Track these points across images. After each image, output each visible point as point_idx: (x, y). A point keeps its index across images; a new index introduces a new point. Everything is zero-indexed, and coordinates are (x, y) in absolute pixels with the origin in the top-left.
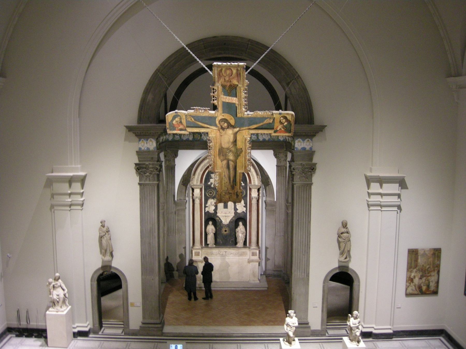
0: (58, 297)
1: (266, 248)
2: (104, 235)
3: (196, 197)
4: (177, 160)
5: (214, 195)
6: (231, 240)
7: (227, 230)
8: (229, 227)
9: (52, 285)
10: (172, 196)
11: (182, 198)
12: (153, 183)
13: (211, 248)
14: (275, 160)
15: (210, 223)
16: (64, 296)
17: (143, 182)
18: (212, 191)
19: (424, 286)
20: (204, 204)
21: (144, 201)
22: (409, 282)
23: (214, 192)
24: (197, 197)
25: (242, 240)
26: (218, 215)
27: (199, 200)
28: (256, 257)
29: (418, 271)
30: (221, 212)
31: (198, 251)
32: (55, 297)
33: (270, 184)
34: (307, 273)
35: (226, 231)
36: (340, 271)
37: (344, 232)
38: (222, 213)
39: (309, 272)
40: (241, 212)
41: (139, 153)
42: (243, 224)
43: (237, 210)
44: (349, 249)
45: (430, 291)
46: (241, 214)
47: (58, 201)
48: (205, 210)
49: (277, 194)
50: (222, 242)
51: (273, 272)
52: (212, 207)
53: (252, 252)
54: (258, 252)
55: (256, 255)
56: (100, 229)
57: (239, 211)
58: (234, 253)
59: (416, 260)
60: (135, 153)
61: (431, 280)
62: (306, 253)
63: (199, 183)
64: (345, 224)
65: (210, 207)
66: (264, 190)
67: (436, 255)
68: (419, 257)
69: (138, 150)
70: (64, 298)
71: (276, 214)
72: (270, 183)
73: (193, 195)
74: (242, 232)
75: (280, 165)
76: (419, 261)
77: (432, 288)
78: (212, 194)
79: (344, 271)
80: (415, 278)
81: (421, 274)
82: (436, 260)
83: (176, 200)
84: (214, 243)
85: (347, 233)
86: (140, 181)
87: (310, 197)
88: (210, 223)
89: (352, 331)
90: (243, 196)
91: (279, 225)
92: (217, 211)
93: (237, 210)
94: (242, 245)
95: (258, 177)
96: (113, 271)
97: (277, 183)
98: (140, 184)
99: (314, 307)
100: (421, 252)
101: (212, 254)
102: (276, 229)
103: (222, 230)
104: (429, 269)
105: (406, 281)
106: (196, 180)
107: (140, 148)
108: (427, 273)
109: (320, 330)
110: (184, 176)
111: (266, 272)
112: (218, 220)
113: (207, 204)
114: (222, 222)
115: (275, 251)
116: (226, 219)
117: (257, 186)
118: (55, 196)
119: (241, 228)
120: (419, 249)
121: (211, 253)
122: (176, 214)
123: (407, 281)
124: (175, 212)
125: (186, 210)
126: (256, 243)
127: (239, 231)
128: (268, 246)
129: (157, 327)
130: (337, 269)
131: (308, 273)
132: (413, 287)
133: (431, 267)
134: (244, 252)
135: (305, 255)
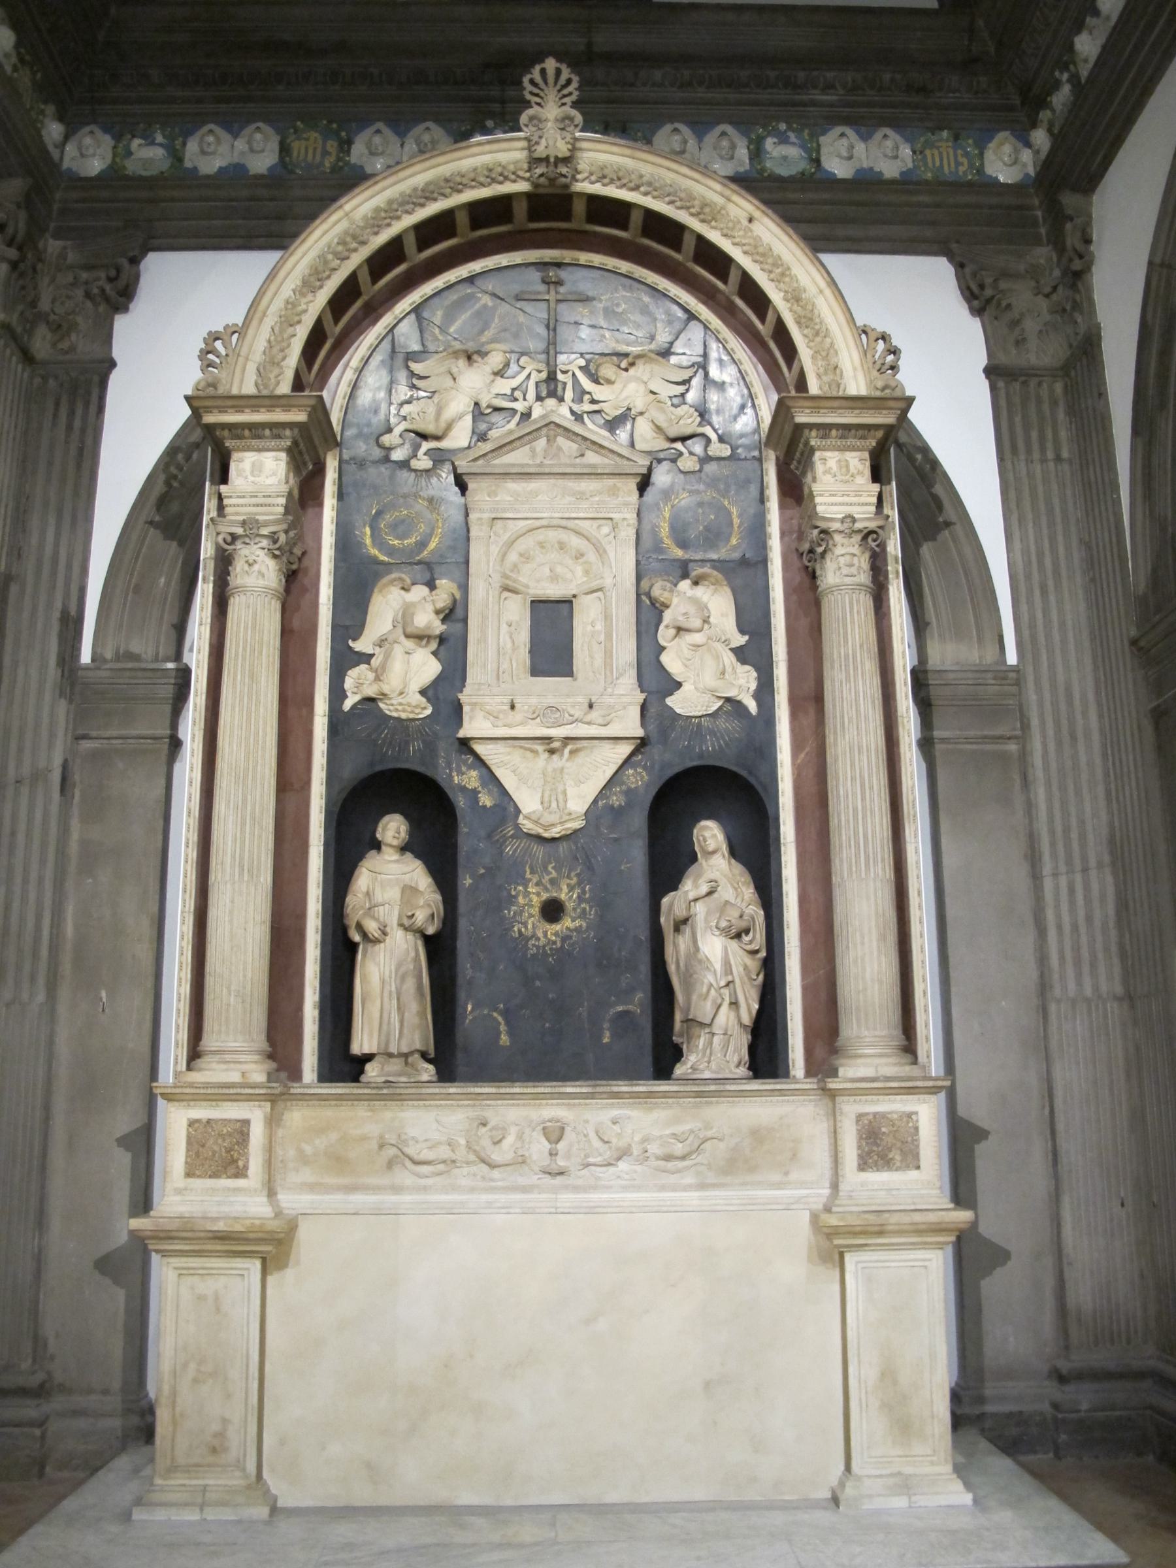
4: (121, 323)
7: (569, 905)
8: (590, 868)
13: (390, 1093)
14: (974, 328)
20: (335, 627)
25: (734, 1004)
28: (913, 1174)
30: (498, 702)
31: (232, 1112)
33: (948, 524)
38: (518, 716)
42: (734, 852)
46: (712, 733)
48: (337, 693)
49: (1024, 607)
50: (511, 1033)
51: (1053, 1391)
53: (860, 1117)
55: (912, 1159)
58: (645, 1140)
65: (387, 656)
72: (953, 517)
83: (86, 657)
91: (1072, 891)
97: (1012, 494)
101: (390, 1165)
110: (180, 457)
111: (981, 1400)
113: (357, 630)
114: (518, 811)
119: (710, 874)
124: (65, 766)
127: (700, 909)
134: (758, 1135)
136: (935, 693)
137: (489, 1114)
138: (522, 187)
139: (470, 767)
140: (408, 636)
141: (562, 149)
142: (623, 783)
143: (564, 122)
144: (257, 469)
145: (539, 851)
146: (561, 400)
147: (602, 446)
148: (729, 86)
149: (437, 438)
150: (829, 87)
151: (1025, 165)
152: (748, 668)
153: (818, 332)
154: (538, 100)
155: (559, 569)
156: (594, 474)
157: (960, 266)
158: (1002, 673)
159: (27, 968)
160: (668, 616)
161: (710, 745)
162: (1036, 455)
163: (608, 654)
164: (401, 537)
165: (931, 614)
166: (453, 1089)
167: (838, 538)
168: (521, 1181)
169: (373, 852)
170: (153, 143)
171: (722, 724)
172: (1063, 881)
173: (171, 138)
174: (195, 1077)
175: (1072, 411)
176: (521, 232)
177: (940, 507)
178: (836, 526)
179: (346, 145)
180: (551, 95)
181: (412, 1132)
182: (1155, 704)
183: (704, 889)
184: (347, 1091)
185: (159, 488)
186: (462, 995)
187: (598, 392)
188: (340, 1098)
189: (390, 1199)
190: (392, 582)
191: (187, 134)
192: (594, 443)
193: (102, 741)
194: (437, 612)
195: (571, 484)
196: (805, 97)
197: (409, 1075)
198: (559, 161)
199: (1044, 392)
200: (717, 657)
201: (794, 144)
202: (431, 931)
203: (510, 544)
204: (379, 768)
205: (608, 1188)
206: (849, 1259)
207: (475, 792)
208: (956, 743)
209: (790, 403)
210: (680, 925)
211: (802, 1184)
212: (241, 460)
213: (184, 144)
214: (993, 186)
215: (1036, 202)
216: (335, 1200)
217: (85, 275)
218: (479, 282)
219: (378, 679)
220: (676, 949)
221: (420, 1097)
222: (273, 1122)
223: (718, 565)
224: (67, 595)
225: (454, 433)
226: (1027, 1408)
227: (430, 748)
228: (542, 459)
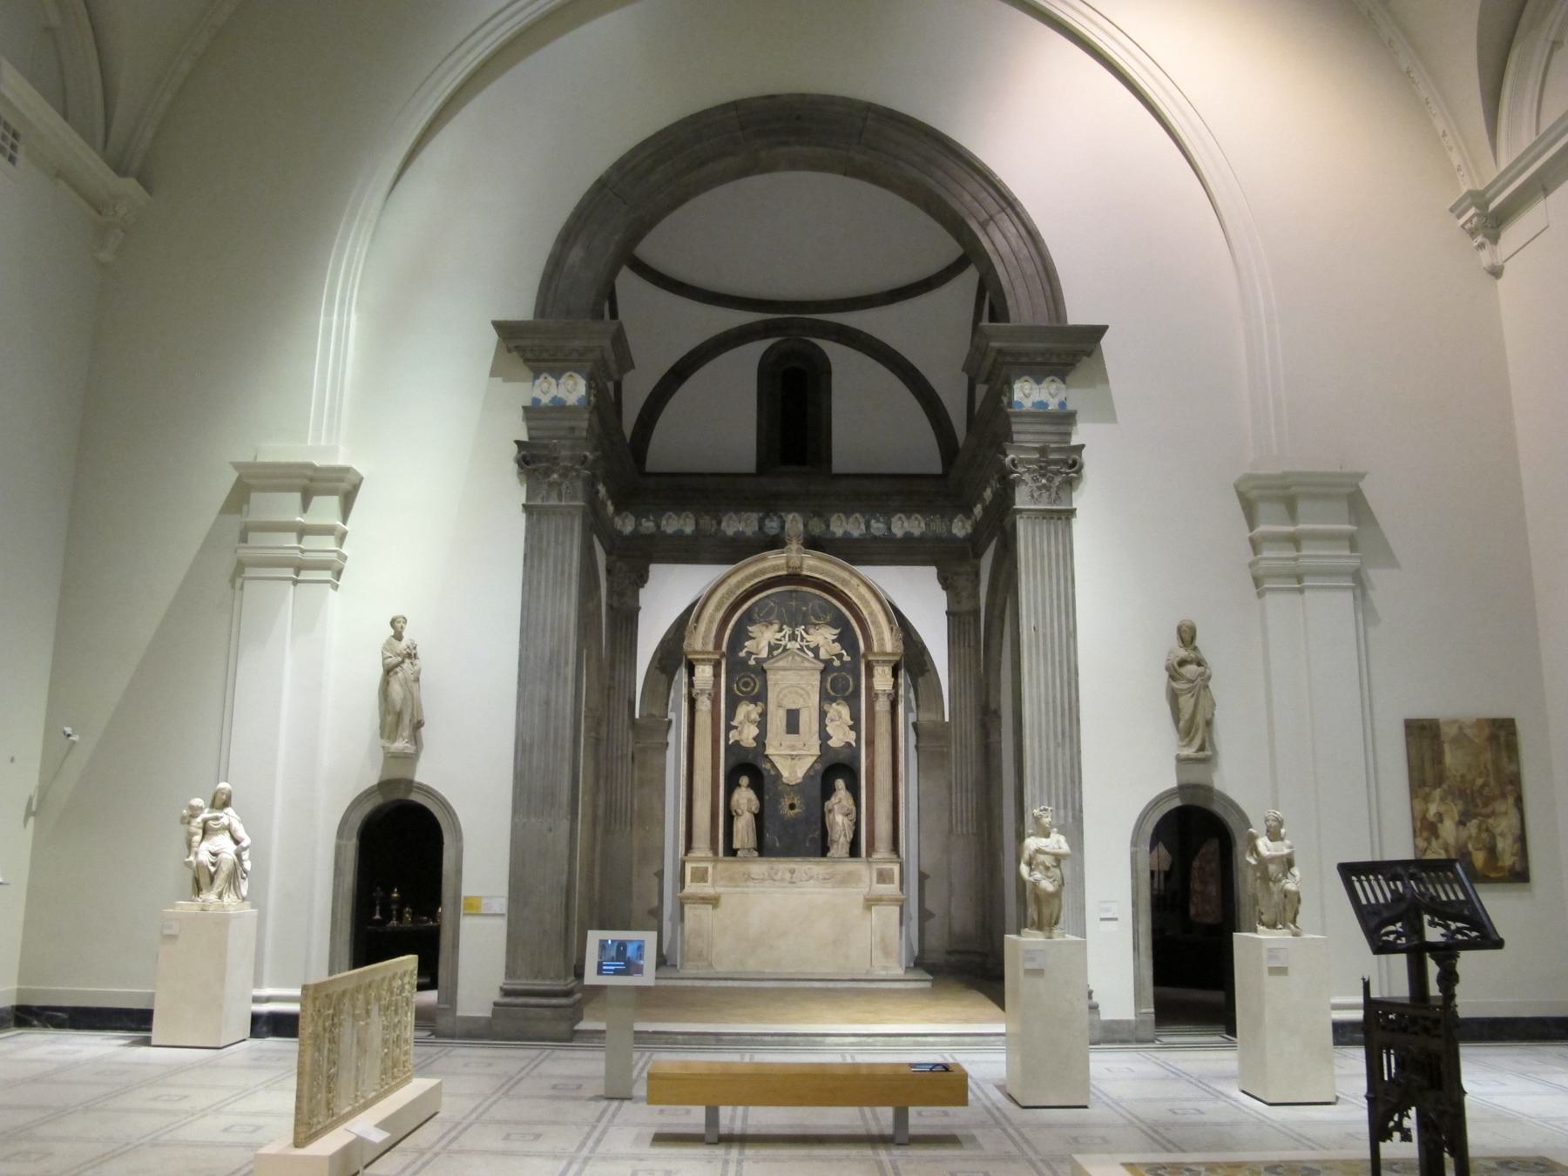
0: (213, 859)
1: (922, 877)
2: (398, 665)
3: (701, 690)
4: (642, 591)
5: (756, 690)
6: (811, 836)
7: (797, 805)
9: (199, 819)
10: (626, 703)
11: (655, 711)
12: (571, 506)
13: (746, 860)
14: (943, 596)
15: (744, 780)
16: (235, 857)
17: (538, 502)
18: (753, 680)
19: (1477, 849)
21: (536, 563)
22: (1425, 834)
24: (702, 691)
25: (845, 836)
26: (769, 751)
27: (709, 699)
28: (891, 886)
29: (1450, 798)
30: (776, 743)
31: (703, 865)
32: (205, 857)
33: (928, 670)
34: (1073, 809)
35: (792, 807)
36: (1185, 803)
37: (1189, 659)
38: (782, 748)
39: (1081, 806)
40: (843, 744)
41: (532, 412)
42: (848, 788)
43: (830, 737)
44: (1209, 716)
45: (1502, 868)
47: (261, 548)
48: (727, 739)
52: (749, 727)
53: (878, 869)
54: (896, 868)
55: (892, 881)
56: (387, 646)
57: (835, 742)
58: (818, 874)
59: (1438, 758)
60: (520, 413)
61: (1498, 830)
62: (1067, 740)
63: (710, 647)
64: (1187, 630)
66: (912, 690)
67: (1502, 740)
68: (1447, 747)
69: (528, 403)
70: (235, 864)
73: (691, 684)
76: (1449, 759)
77: (1508, 859)
79: (1199, 802)
80: (1441, 821)
81: (1460, 805)
82: (1505, 760)
83: (637, 716)
85: (1199, 664)
86: (528, 498)
87: (1068, 542)
88: (744, 780)
89: (1268, 885)
90: (847, 693)
93: (830, 737)
94: (844, 851)
95: (892, 629)
96: (416, 797)
98: (527, 508)
99: (1102, 919)
100: (1448, 732)
102: (951, 814)
104: (1486, 790)
105: (1415, 831)
107: (536, 401)
108: (1480, 805)
109: (1132, 1021)
114: (782, 776)
115: (951, 885)
116: (795, 765)
117: (889, 654)
118: (251, 535)
120: (1441, 721)
121: (744, 874)
122: (636, 761)
123: (1418, 833)
125: (668, 752)
126: (891, 842)
128: (927, 871)
129: (554, 1007)
130: (1175, 794)
131: (1077, 807)
132: (1439, 854)
133: (1492, 782)
134: (850, 874)
135: (1064, 746)
138: (784, 573)
141: (798, 563)
143: (798, 551)
145: (788, 789)
146: (796, 641)
148: (839, 578)
156: (806, 669)
157: (938, 569)
158: (944, 725)
159: (623, 819)
160: (829, 715)
161: (841, 757)
162: (962, 644)
163: (810, 728)
164: (746, 688)
165: (920, 703)
166: (764, 859)
167: (880, 696)
177: (926, 665)
179: (719, 523)
180: (794, 542)
183: (837, 801)
186: (765, 831)
189: (746, 890)
202: (756, 812)
203: (780, 692)
206: (873, 908)
207: (769, 770)
210: (830, 811)
211: (861, 888)
214: (954, 539)
219: (740, 734)
221: (755, 861)
222: (714, 868)
224: (630, 691)
225: (763, 652)
228: (794, 546)
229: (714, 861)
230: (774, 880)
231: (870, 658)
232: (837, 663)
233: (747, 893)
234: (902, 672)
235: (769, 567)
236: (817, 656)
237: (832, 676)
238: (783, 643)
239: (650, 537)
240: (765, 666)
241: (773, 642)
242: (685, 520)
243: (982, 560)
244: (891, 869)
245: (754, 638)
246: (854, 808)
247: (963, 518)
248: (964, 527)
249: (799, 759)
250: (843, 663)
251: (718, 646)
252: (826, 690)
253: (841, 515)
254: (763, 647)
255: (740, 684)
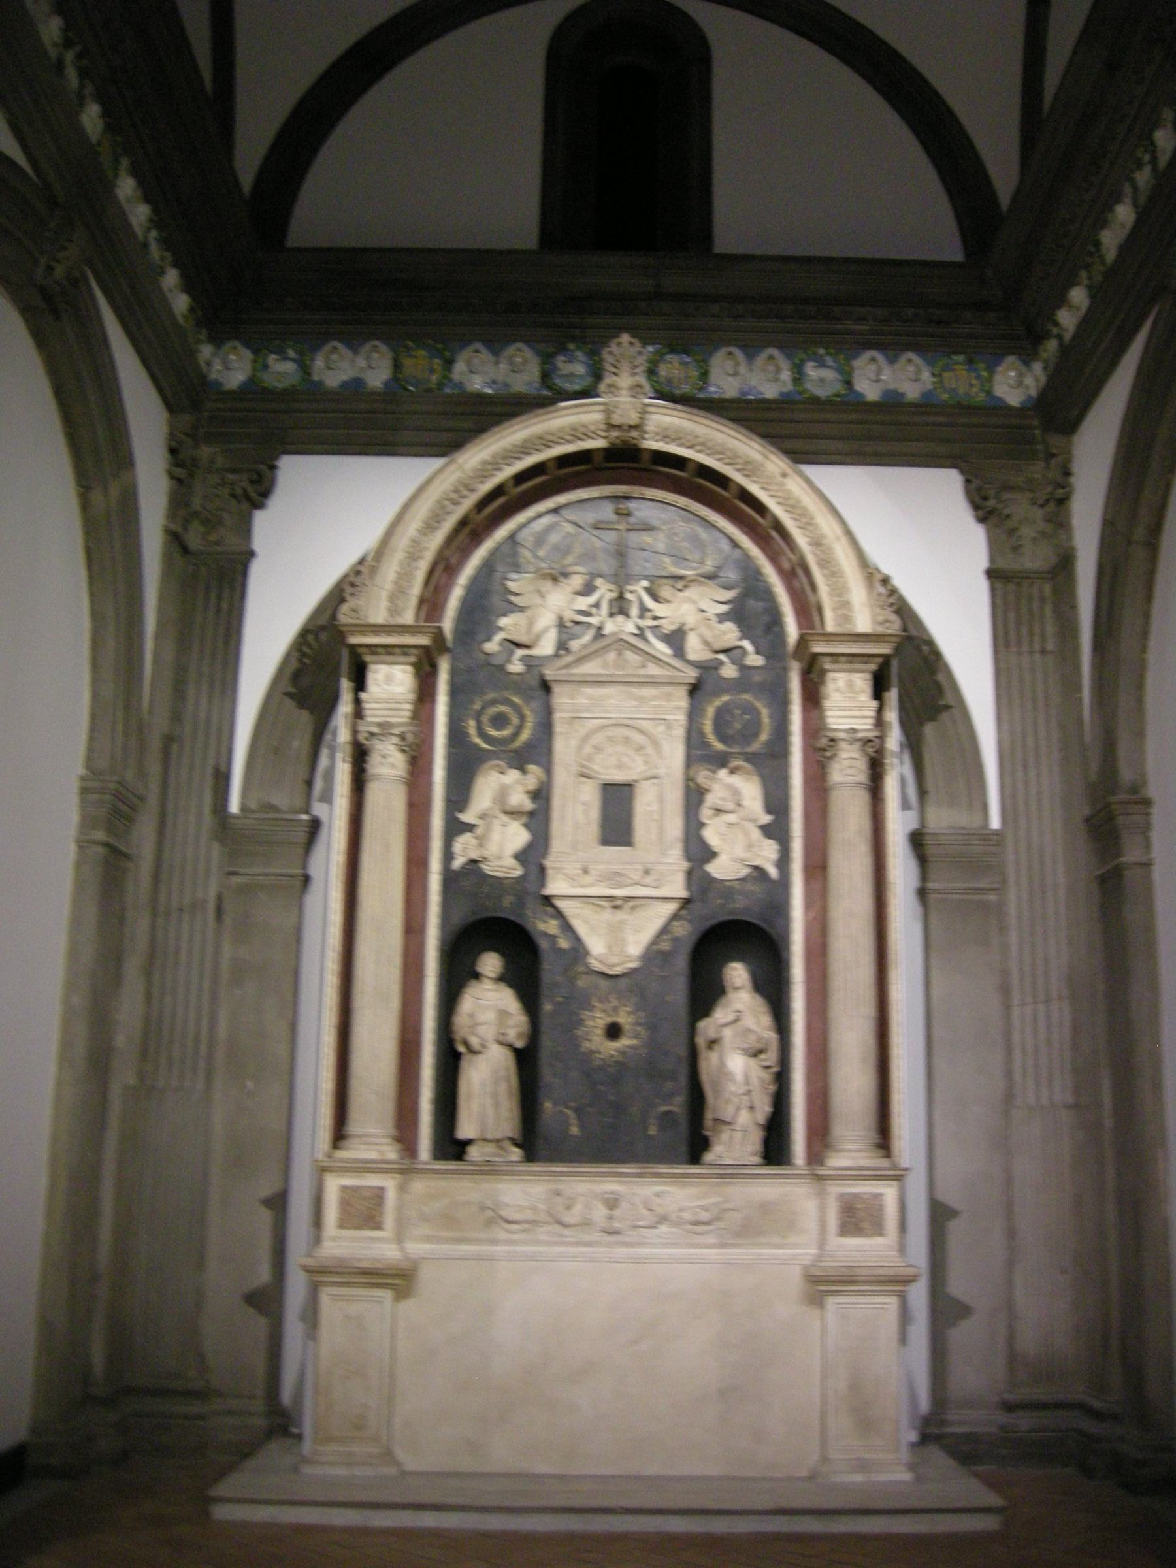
3: (380, 725)
4: (262, 521)
5: (525, 735)
11: (281, 799)
13: (489, 1170)
15: (490, 963)
23: (527, 712)
26: (555, 886)
28: (879, 1241)
30: (572, 868)
31: (373, 1181)
33: (947, 707)
35: (613, 1031)
38: (588, 879)
40: (744, 872)
48: (448, 856)
50: (582, 1126)
51: (1002, 1418)
53: (841, 1196)
55: (878, 1229)
65: (488, 829)
71: (1003, 929)
73: (358, 713)
74: (753, 1037)
75: (1016, 567)
78: (506, 733)
83: (234, 807)
84: (485, 868)
88: (490, 963)
91: (1035, 1019)
92: (548, 863)
101: (489, 1223)
103: (580, 1022)
106: (384, 595)
111: (943, 1423)
112: (553, 938)
114: (587, 953)
121: (483, 1208)
122: (228, 919)
124: (220, 899)
127: (727, 1033)
128: (950, 1195)
134: (766, 1208)
136: (930, 851)
137: (561, 1187)
138: (600, 443)
139: (553, 917)
140: (506, 813)
141: (633, 418)
142: (670, 932)
143: (636, 389)
144: (389, 679)
145: (604, 984)
146: (627, 615)
147: (660, 660)
149: (527, 647)
150: (861, 319)
151: (1027, 388)
152: (771, 842)
153: (834, 573)
154: (615, 370)
155: (625, 760)
156: (652, 682)
162: (1025, 648)
163: (661, 830)
165: (930, 785)
167: (843, 745)
168: (587, 1238)
169: (473, 983)
170: (286, 358)
171: (750, 887)
172: (1028, 1009)
173: (301, 353)
174: (341, 1154)
175: (1056, 611)
176: (598, 469)
178: (842, 735)
179: (449, 363)
181: (506, 1199)
182: (1100, 872)
183: (731, 1017)
184: (457, 1167)
185: (294, 664)
187: (658, 609)
188: (446, 1172)
190: (492, 768)
191: (315, 349)
192: (654, 657)
193: (246, 877)
194: (528, 792)
195: (636, 691)
196: (839, 327)
197: (501, 1156)
198: (632, 427)
199: (1035, 591)
200: (747, 833)
201: (829, 367)
202: (520, 1044)
203: (586, 739)
204: (478, 917)
205: (652, 1245)
208: (945, 893)
209: (807, 637)
210: (712, 1043)
212: (375, 672)
213: (312, 360)
214: (999, 408)
215: (1036, 422)
216: (445, 1249)
217: (230, 476)
218: (564, 512)
219: (481, 846)
220: (709, 1062)
221: (513, 1173)
222: (402, 1189)
223: (751, 758)
224: (218, 753)
226: (979, 1430)
227: (521, 902)
229: (402, 1172)
230: (565, 1225)
231: (818, 648)
232: (729, 671)
233: (491, 1259)
234: (892, 696)
235: (561, 429)
236: (679, 651)
237: (718, 702)
238: (593, 620)
239: (287, 395)
240: (549, 673)
241: (569, 615)
242: (368, 358)
243: (1076, 439)
244: (878, 1196)
245: (522, 609)
246: (772, 1036)
247: (1018, 363)
248: (1020, 384)
249: (633, 908)
250: (743, 668)
251: (431, 604)
252: (702, 734)
253: (736, 351)
254: (546, 630)
255: (485, 719)
